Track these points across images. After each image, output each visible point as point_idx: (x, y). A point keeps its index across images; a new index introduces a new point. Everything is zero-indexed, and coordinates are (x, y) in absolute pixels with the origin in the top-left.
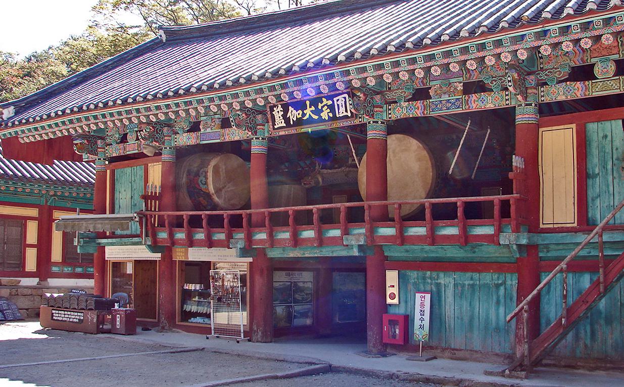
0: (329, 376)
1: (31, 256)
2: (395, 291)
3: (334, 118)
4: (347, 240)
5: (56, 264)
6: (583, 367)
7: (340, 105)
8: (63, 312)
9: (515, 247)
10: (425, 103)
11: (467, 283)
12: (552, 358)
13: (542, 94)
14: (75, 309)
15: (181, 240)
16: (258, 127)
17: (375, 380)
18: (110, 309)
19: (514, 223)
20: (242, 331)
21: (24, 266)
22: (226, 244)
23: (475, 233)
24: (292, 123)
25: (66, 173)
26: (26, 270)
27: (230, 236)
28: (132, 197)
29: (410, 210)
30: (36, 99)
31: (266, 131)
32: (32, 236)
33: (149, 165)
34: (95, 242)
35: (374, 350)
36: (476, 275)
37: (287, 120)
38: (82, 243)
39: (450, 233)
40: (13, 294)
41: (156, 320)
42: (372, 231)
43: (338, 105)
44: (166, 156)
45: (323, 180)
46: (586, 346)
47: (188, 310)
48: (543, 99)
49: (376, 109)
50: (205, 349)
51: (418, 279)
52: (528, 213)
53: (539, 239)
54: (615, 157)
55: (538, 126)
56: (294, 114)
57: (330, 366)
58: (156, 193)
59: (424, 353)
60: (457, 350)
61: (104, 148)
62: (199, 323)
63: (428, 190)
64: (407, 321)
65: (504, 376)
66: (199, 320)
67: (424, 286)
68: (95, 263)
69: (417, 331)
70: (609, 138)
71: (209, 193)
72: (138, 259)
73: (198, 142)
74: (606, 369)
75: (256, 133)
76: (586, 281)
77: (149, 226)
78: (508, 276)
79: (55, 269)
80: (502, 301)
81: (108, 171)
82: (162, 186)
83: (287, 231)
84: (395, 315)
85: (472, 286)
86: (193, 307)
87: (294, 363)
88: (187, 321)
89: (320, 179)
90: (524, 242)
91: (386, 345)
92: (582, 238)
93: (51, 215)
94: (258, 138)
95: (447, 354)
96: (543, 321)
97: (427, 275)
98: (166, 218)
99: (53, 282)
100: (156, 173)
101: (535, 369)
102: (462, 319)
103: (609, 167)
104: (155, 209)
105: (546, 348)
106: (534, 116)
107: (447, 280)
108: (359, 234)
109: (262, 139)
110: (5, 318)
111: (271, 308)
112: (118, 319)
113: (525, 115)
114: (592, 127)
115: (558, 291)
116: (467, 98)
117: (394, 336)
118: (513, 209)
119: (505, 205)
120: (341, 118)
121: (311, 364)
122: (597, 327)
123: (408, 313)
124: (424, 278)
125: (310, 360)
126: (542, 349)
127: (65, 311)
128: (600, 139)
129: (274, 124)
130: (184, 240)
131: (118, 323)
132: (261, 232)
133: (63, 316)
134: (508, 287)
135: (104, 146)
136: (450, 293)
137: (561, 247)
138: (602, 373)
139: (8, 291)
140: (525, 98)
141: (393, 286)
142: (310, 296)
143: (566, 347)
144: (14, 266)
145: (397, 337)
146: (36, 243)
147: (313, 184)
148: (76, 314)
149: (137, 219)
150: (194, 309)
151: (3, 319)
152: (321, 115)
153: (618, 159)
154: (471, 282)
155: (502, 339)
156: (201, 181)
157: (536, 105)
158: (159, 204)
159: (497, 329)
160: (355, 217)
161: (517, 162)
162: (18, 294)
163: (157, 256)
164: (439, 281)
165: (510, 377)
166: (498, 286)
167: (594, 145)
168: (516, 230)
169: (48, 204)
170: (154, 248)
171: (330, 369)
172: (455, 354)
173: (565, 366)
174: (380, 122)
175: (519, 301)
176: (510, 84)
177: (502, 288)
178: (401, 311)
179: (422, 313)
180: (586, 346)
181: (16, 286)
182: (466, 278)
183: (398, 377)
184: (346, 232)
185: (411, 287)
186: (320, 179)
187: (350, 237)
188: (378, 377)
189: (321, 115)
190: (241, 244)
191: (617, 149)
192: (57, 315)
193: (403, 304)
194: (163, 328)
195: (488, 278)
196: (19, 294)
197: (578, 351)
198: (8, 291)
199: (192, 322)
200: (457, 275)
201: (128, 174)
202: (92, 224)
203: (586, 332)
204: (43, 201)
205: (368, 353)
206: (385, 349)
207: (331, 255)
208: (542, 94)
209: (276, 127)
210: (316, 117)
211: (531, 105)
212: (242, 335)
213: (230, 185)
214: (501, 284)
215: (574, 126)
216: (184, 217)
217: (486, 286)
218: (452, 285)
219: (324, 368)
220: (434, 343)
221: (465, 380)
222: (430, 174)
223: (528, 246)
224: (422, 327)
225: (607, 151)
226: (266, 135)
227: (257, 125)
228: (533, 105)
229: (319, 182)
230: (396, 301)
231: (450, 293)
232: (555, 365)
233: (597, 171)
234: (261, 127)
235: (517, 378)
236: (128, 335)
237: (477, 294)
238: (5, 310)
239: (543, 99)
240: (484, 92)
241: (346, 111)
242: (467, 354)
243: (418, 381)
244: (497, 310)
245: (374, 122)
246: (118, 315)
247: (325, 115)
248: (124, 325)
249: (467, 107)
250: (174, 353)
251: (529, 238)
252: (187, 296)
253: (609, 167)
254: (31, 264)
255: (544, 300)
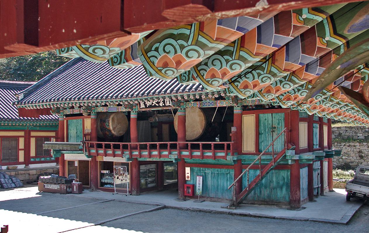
0: (165, 210)
1: (21, 154)
2: (189, 175)
3: (165, 106)
4: (170, 156)
5: (33, 157)
6: (257, 204)
7: (167, 101)
8: (49, 185)
9: (232, 161)
10: (200, 103)
11: (216, 172)
12: (246, 200)
13: (244, 102)
14: (56, 183)
15: (101, 153)
16: (133, 107)
17: (182, 211)
18: (71, 183)
19: (232, 152)
20: (128, 191)
21: (18, 160)
22: (121, 156)
23: (218, 155)
24: (147, 106)
25: (9, 93)
26: (19, 161)
27: (123, 153)
28: (77, 133)
29: (196, 137)
30: (32, 89)
31: (137, 108)
32: (22, 145)
33: (85, 119)
34: (60, 152)
35: (181, 198)
36: (219, 170)
37: (146, 105)
38: (55, 153)
39: (209, 155)
40: (16, 174)
41: (89, 186)
42: (180, 153)
43: (166, 101)
44: (93, 116)
45: (158, 119)
46: (258, 196)
47: (103, 182)
48: (244, 104)
49: (181, 104)
50: (115, 200)
51: (198, 171)
52: (238, 149)
53: (242, 157)
54: (269, 127)
55: (242, 114)
56: (148, 103)
57: (165, 206)
58: (89, 132)
59: (200, 199)
60: (212, 198)
61: (63, 110)
62: (109, 187)
63: (203, 129)
64: (194, 187)
65: (227, 208)
66: (108, 186)
67: (200, 173)
68: (59, 160)
69: (197, 191)
70: (267, 120)
71: (110, 130)
72: (80, 160)
73: (107, 111)
74: (265, 204)
75: (132, 109)
76: (258, 172)
77: (87, 148)
78: (231, 170)
79: (32, 160)
80: (229, 179)
81: (65, 121)
82: (92, 129)
83: (147, 152)
84: (189, 184)
85: (218, 174)
86: (106, 180)
87: (151, 205)
88: (103, 186)
89: (157, 119)
90: (235, 159)
91: (186, 196)
92: (257, 157)
93: (30, 134)
94: (134, 112)
95: (209, 199)
96: (243, 187)
97: (201, 169)
98: (95, 144)
99: (32, 166)
100: (88, 123)
101: (240, 205)
102: (214, 186)
103: (267, 131)
104: (89, 139)
105: (242, 198)
106: (240, 111)
107: (208, 171)
108: (175, 154)
109: (135, 112)
110: (16, 186)
111: (139, 181)
112: (75, 188)
113: (237, 110)
114: (261, 115)
115: (250, 175)
116: (216, 102)
117: (189, 193)
118: (231, 147)
119: (229, 146)
120: (167, 106)
121: (158, 205)
122: (262, 190)
123: (194, 184)
124: (200, 170)
125: (157, 204)
126: (241, 199)
127: (50, 184)
128: (264, 120)
129: (140, 106)
130: (102, 153)
131: (75, 189)
132: (136, 151)
133: (50, 186)
134: (231, 174)
135: (63, 110)
136: (210, 176)
137: (249, 160)
138: (263, 206)
139: (14, 173)
140: (237, 104)
141: (188, 173)
142: (154, 174)
143: (251, 197)
144: (14, 160)
145: (190, 193)
146: (23, 148)
147: (154, 120)
148: (56, 185)
149: (82, 145)
150: (106, 181)
151: (15, 186)
152: (160, 104)
153: (270, 128)
154: (217, 172)
155: (229, 194)
156: (107, 124)
157: (241, 107)
158: (90, 138)
159: (227, 190)
160: (173, 147)
161: (233, 129)
162: (18, 174)
163: (90, 159)
164: (205, 172)
165: (230, 209)
166: (227, 174)
167: (262, 122)
168: (233, 155)
169: (29, 129)
170: (89, 156)
171: (165, 207)
172: (212, 200)
173: (251, 204)
174: (183, 109)
175: (235, 180)
176: (231, 101)
177: (229, 175)
178: (192, 183)
179: (199, 184)
180: (258, 196)
181: (15, 169)
182: (216, 171)
183: (190, 210)
184: (170, 153)
185: (195, 174)
186: (157, 119)
187: (171, 155)
188: (183, 210)
189: (160, 104)
190: (128, 156)
191: (270, 124)
192: (47, 186)
193: (192, 180)
194: (93, 190)
195: (224, 170)
196: (19, 174)
197: (255, 198)
198: (14, 173)
199: (105, 187)
200: (212, 170)
201: (74, 122)
202: (62, 146)
203: (258, 191)
204: (26, 128)
205: (179, 199)
206: (185, 198)
207: (164, 160)
208: (244, 102)
209: (141, 107)
210: (158, 105)
211: (239, 106)
212: (128, 192)
213: (119, 125)
214: (228, 173)
215: (255, 115)
216: (103, 144)
217: (223, 174)
218: (210, 173)
219: (163, 207)
220: (204, 195)
221: (214, 211)
222: (204, 123)
223: (238, 160)
224: (199, 189)
225: (266, 125)
226: (137, 110)
227: (133, 106)
228: (240, 106)
229: (156, 120)
230: (189, 179)
231: (210, 176)
232: (247, 203)
233: (262, 132)
234: (135, 107)
235: (232, 209)
236: (80, 194)
237: (220, 177)
238: (15, 182)
239: (244, 104)
240: (223, 100)
241: (170, 104)
242: (216, 199)
243: (197, 211)
244: (227, 183)
245: (180, 109)
246: (75, 186)
247: (161, 104)
248: (77, 190)
249: (216, 105)
250: (103, 202)
251: (237, 158)
252: (102, 175)
253: (267, 131)
254: (21, 159)
255: (244, 179)
